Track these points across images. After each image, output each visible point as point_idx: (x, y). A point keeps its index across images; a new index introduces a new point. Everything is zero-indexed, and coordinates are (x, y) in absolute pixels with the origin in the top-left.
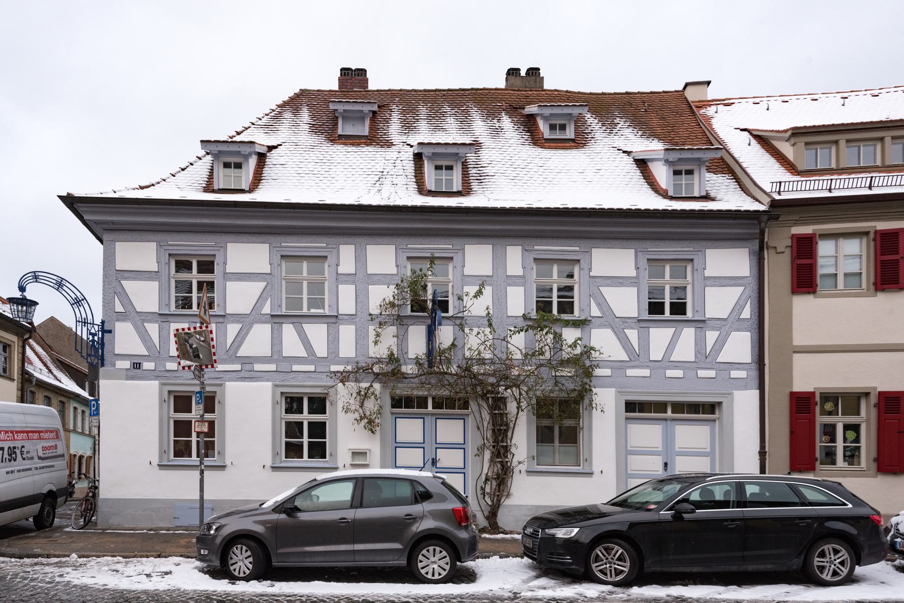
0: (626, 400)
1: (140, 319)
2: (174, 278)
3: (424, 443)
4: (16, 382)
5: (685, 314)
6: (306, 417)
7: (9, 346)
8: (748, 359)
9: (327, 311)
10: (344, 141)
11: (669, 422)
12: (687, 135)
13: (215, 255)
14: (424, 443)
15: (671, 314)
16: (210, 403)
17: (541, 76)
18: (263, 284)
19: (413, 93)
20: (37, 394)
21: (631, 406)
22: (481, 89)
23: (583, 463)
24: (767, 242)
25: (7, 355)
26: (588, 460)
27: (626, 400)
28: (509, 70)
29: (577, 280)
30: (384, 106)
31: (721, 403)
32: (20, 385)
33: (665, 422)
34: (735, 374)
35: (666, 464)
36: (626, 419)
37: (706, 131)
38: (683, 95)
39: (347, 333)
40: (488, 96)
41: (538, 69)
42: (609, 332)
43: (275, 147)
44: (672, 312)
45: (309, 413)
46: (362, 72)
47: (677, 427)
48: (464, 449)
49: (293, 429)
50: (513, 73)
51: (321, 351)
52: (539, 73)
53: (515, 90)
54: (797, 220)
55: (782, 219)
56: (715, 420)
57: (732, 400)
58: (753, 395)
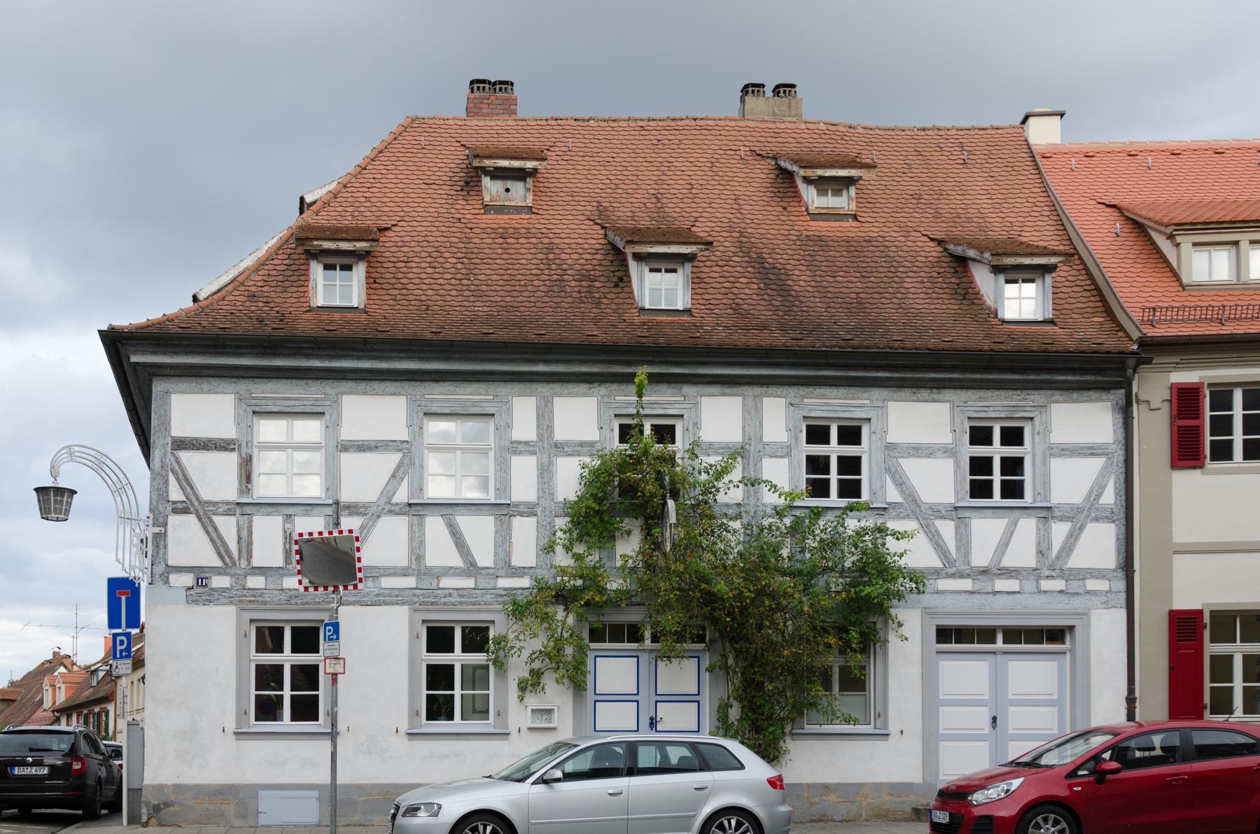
0: (937, 626)
3: (638, 694)
5: (1021, 497)
6: (288, 658)
10: (495, 216)
12: (1028, 210)
14: (638, 694)
15: (1002, 498)
18: (397, 457)
21: (944, 634)
23: (875, 720)
24: (1136, 394)
26: (882, 715)
27: (937, 626)
34: (1092, 585)
35: (994, 719)
37: (1056, 203)
38: (1021, 135)
42: (192, 518)
43: (386, 229)
44: (1004, 495)
45: (293, 651)
47: (1011, 663)
48: (698, 702)
51: (485, 557)
54: (1177, 364)
56: (1065, 653)
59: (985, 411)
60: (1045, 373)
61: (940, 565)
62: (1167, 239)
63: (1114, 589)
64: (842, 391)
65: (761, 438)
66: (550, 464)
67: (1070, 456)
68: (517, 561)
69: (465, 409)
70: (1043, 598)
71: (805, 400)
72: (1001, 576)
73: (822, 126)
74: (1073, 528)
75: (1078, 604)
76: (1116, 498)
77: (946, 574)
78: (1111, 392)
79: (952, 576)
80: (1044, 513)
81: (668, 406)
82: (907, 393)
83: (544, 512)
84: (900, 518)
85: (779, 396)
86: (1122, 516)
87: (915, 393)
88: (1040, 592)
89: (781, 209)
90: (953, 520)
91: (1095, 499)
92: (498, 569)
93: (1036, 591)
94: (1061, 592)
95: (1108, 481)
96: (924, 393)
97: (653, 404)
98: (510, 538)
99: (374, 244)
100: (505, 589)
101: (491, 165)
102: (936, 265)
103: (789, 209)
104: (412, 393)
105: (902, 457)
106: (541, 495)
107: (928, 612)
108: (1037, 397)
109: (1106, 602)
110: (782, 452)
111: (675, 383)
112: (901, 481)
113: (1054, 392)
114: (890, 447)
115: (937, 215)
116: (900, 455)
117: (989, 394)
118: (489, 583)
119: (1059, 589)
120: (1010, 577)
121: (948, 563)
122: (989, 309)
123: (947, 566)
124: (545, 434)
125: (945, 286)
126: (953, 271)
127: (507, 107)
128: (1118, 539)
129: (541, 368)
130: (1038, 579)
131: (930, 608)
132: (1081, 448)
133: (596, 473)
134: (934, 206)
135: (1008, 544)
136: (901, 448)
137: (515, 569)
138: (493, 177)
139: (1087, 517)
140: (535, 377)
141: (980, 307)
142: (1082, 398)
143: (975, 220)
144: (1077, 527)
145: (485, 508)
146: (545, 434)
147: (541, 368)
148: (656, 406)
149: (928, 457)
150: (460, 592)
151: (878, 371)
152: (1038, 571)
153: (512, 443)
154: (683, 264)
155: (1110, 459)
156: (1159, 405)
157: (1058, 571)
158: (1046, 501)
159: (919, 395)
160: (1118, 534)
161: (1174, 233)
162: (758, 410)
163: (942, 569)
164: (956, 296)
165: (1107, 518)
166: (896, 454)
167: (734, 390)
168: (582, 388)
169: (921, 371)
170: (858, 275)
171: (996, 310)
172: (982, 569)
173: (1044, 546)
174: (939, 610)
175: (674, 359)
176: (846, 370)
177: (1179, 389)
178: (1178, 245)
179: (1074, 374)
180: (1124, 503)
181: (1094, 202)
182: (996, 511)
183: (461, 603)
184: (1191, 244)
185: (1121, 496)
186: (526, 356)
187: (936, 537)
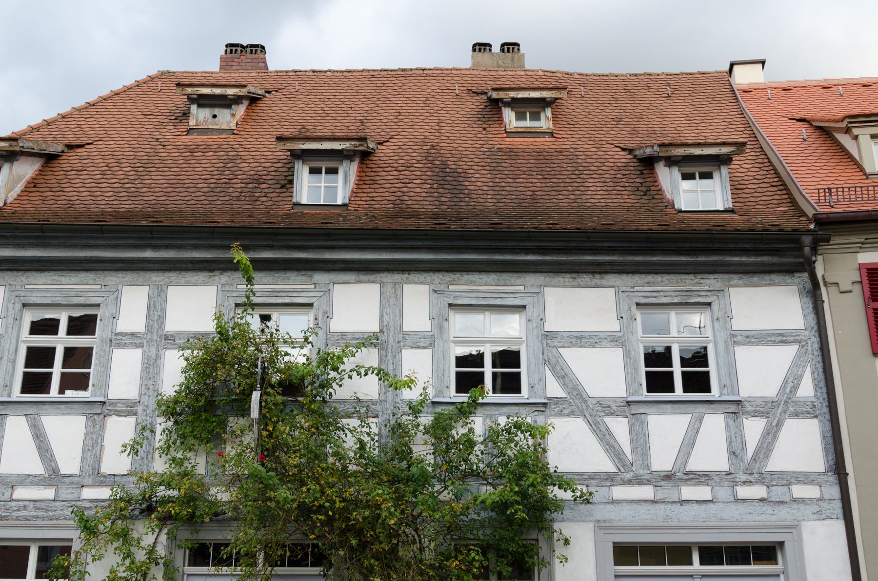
2: (642, 342)
5: (708, 390)
15: (685, 391)
19: (345, 74)
34: (799, 491)
36: (616, 576)
40: (437, 78)
41: (517, 45)
46: (258, 49)
54: (863, 243)
56: (778, 576)
57: (800, 539)
59: (655, 297)
60: (715, 254)
61: (613, 469)
62: (846, 133)
63: (826, 497)
64: (492, 277)
65: (401, 327)
66: (158, 357)
67: (757, 344)
68: (106, 468)
69: (68, 299)
70: (741, 508)
71: (451, 287)
72: (688, 482)
73: (541, 73)
74: (769, 427)
75: (784, 514)
76: (816, 390)
77: (622, 479)
78: (796, 275)
79: (629, 482)
80: (733, 408)
81: (295, 294)
82: (566, 278)
83: (145, 411)
84: (564, 415)
85: (421, 283)
86: (826, 410)
87: (575, 278)
88: (737, 500)
89: (481, 129)
90: (627, 417)
91: (791, 392)
92: (84, 477)
93: (732, 499)
94: (762, 500)
95: (804, 372)
96: (585, 279)
97: (278, 292)
98: (102, 441)
99: (13, 143)
100: (91, 501)
101: (193, 93)
102: (622, 168)
103: (488, 129)
104: (12, 283)
105: (564, 347)
106: (144, 391)
107: (602, 527)
108: (713, 281)
109: (819, 512)
110: (425, 342)
111: (305, 270)
112: (562, 373)
113: (731, 276)
114: (549, 336)
115: (634, 132)
116: (561, 344)
117: (659, 278)
118: (72, 493)
119: (759, 497)
120: (700, 483)
121: (623, 466)
122: (668, 202)
123: (623, 470)
124: (156, 325)
125: (627, 184)
126: (639, 173)
127: (256, 64)
128: (824, 437)
129: (149, 254)
130: (734, 484)
131: (605, 521)
132: (768, 335)
133: (203, 362)
134: (633, 126)
135: (693, 444)
136: (562, 337)
137: (105, 476)
138: (200, 106)
139: (785, 412)
140: (147, 265)
141: (660, 201)
142: (764, 282)
143: (670, 135)
144: (774, 423)
145: (75, 406)
146: (156, 325)
147: (149, 254)
148: (282, 294)
149: (594, 347)
150: (38, 504)
151: (527, 254)
152: (733, 476)
153: (117, 334)
154: (342, 161)
155: (803, 346)
156: (850, 288)
157: (756, 476)
158: (733, 394)
159: (580, 280)
160: (823, 432)
161: (849, 125)
162: (399, 298)
163: (616, 474)
164: (638, 193)
165: (808, 413)
166: (556, 344)
167: (372, 277)
168: (202, 276)
169: (576, 254)
170: (540, 177)
171: (673, 201)
172: (666, 473)
173: (736, 446)
174: (615, 524)
175: (297, 243)
176: (489, 253)
177: (868, 269)
178: (856, 138)
179: (748, 256)
180: (825, 396)
181: (787, 119)
182: (676, 406)
183: (36, 517)
184: (869, 137)
185: (821, 388)
186: (131, 241)
187: (608, 436)
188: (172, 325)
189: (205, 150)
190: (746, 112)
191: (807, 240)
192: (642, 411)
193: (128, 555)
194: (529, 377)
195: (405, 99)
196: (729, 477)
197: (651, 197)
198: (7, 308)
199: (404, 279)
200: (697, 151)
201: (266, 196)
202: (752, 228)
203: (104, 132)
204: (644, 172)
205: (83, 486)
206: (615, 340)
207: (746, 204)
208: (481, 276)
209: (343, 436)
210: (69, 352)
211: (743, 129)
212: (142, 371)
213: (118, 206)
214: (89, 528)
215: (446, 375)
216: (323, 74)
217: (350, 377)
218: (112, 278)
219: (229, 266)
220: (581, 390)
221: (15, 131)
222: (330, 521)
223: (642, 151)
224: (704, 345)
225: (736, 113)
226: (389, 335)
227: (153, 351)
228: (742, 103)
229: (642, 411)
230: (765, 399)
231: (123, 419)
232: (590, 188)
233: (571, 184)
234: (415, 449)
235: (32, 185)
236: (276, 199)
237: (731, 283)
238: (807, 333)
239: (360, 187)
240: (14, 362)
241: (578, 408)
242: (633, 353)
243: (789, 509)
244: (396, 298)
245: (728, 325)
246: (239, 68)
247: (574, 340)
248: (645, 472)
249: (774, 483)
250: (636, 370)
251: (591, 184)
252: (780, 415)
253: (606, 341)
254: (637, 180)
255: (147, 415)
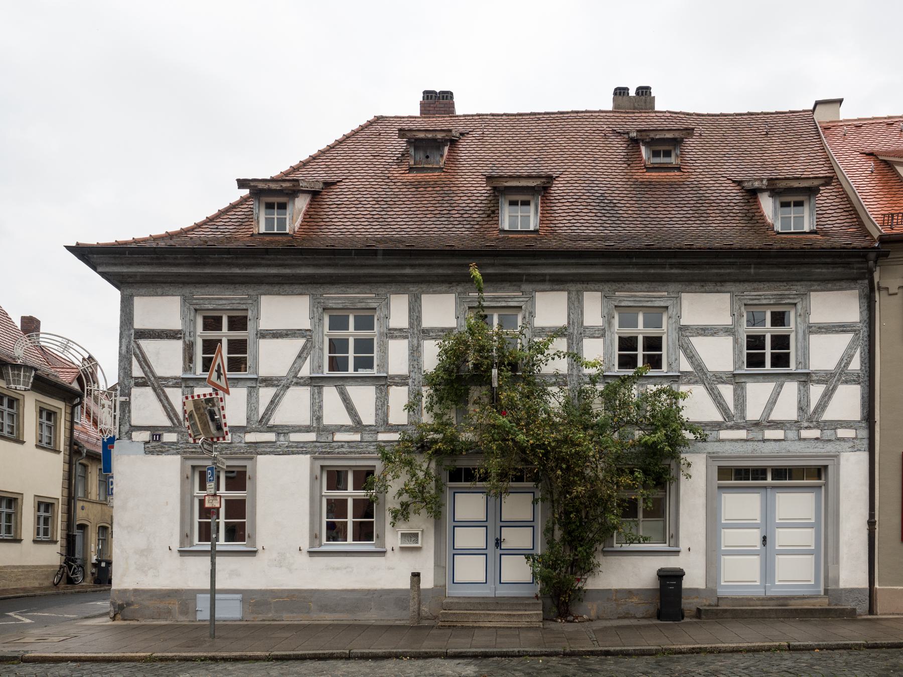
1: (158, 385)
4: (62, 454)
7: (55, 413)
8: (858, 417)
9: (374, 372)
10: (415, 175)
11: (769, 490)
13: (247, 310)
16: (238, 479)
17: (652, 95)
20: (90, 468)
22: (582, 112)
25: (51, 423)
26: (675, 537)
28: (616, 89)
29: (665, 331)
30: (468, 134)
31: (826, 467)
32: (67, 457)
33: (763, 491)
34: (842, 433)
35: (764, 539)
39: (399, 396)
40: (589, 120)
43: (334, 184)
46: (447, 96)
48: (533, 527)
49: (336, 508)
50: (620, 92)
51: (368, 417)
52: (650, 93)
53: (622, 112)
55: (893, 256)
57: (839, 464)
58: (863, 457)
61: (721, 419)
63: (859, 436)
66: (419, 345)
67: (826, 333)
68: (392, 420)
70: (802, 444)
71: (616, 293)
75: (830, 448)
76: (862, 365)
82: (696, 286)
83: (414, 382)
84: (690, 383)
87: (703, 286)
88: (800, 439)
90: (732, 384)
91: (844, 366)
92: (378, 427)
93: (797, 438)
94: (817, 439)
95: (855, 352)
100: (384, 442)
104: (314, 293)
105: (693, 336)
107: (712, 457)
112: (691, 355)
113: (812, 283)
114: (683, 329)
116: (691, 334)
118: (372, 437)
119: (815, 437)
121: (728, 417)
123: (727, 420)
124: (415, 323)
126: (747, 201)
128: (863, 398)
131: (713, 453)
132: (834, 326)
135: (775, 402)
136: (692, 329)
137: (392, 426)
139: (839, 380)
141: (763, 225)
142: (835, 288)
144: (831, 388)
146: (415, 323)
148: (500, 299)
149: (713, 336)
153: (390, 330)
155: (857, 334)
157: (815, 423)
158: (805, 369)
159: (706, 288)
162: (580, 302)
163: (723, 422)
167: (562, 287)
171: (773, 225)
172: (755, 422)
174: (720, 455)
180: (868, 369)
183: (351, 452)
185: (865, 364)
187: (719, 398)
188: (426, 323)
189: (426, 186)
190: (827, 148)
191: (872, 256)
192: (743, 380)
193: (414, 475)
194: (668, 357)
195: (566, 139)
196: (796, 424)
197: (755, 222)
198: (313, 311)
199: (584, 287)
200: (796, 184)
201: (478, 224)
202: (833, 246)
203: (348, 171)
204: (750, 200)
205: (378, 432)
206: (729, 331)
207: (835, 225)
208: (637, 285)
209: (549, 399)
210: (774, 338)
211: (824, 163)
212: (409, 355)
213: (375, 233)
214: (386, 458)
215: (613, 357)
216: (500, 118)
217: (553, 359)
218: (382, 289)
219: (468, 279)
220: (703, 366)
221: (282, 171)
222: (546, 454)
223: (750, 183)
224: (763, 334)
225: (819, 148)
226: (574, 329)
227: (415, 342)
228: (824, 139)
229: (743, 380)
230: (826, 372)
231: (399, 388)
232: (711, 215)
233: (697, 212)
234: (593, 407)
235: (308, 216)
236: (486, 226)
237: (813, 288)
238: (861, 325)
239: (544, 215)
240: (322, 349)
241: (700, 378)
242: (740, 340)
243: (833, 445)
244: (579, 302)
245: (807, 320)
246: (435, 112)
247: (700, 331)
248: (742, 421)
249: (826, 428)
250: (741, 352)
251: (712, 212)
252: (836, 382)
253: (722, 332)
254: (745, 208)
255: (415, 385)
